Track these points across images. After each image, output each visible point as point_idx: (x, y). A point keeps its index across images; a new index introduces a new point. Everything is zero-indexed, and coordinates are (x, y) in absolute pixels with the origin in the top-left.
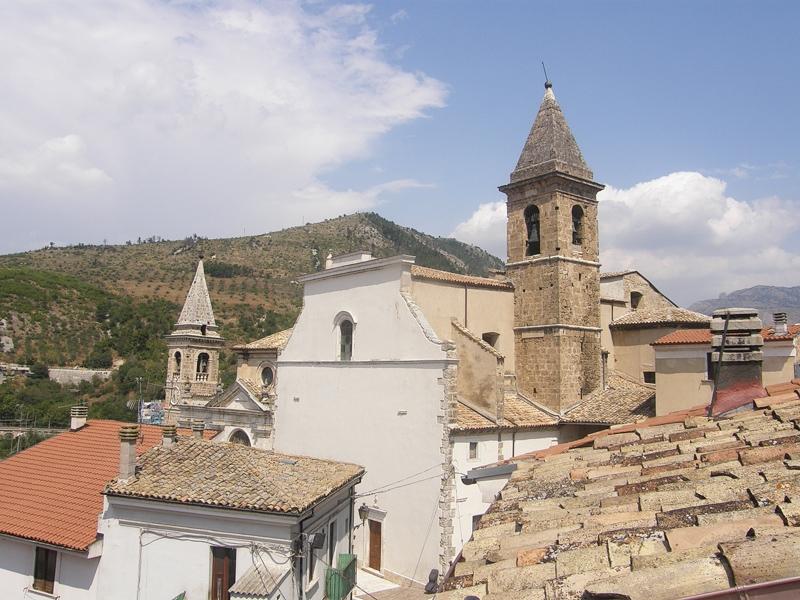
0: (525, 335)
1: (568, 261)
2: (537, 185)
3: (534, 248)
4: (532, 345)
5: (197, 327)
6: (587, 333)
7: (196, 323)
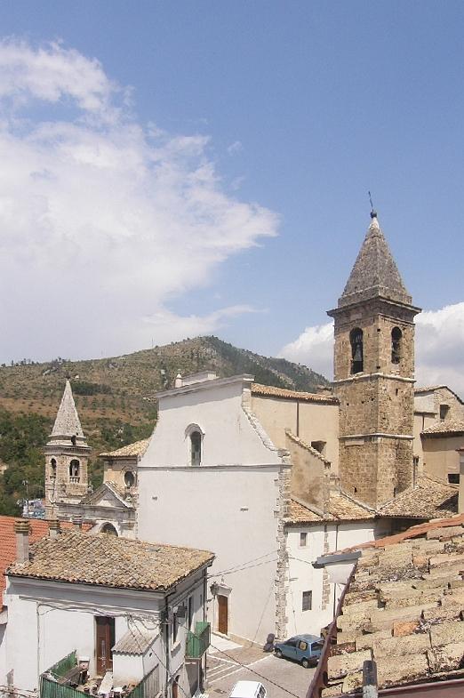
0: (347, 443)
1: (387, 378)
2: (362, 310)
3: (358, 367)
4: (354, 452)
5: (68, 438)
6: (401, 441)
7: (67, 434)
